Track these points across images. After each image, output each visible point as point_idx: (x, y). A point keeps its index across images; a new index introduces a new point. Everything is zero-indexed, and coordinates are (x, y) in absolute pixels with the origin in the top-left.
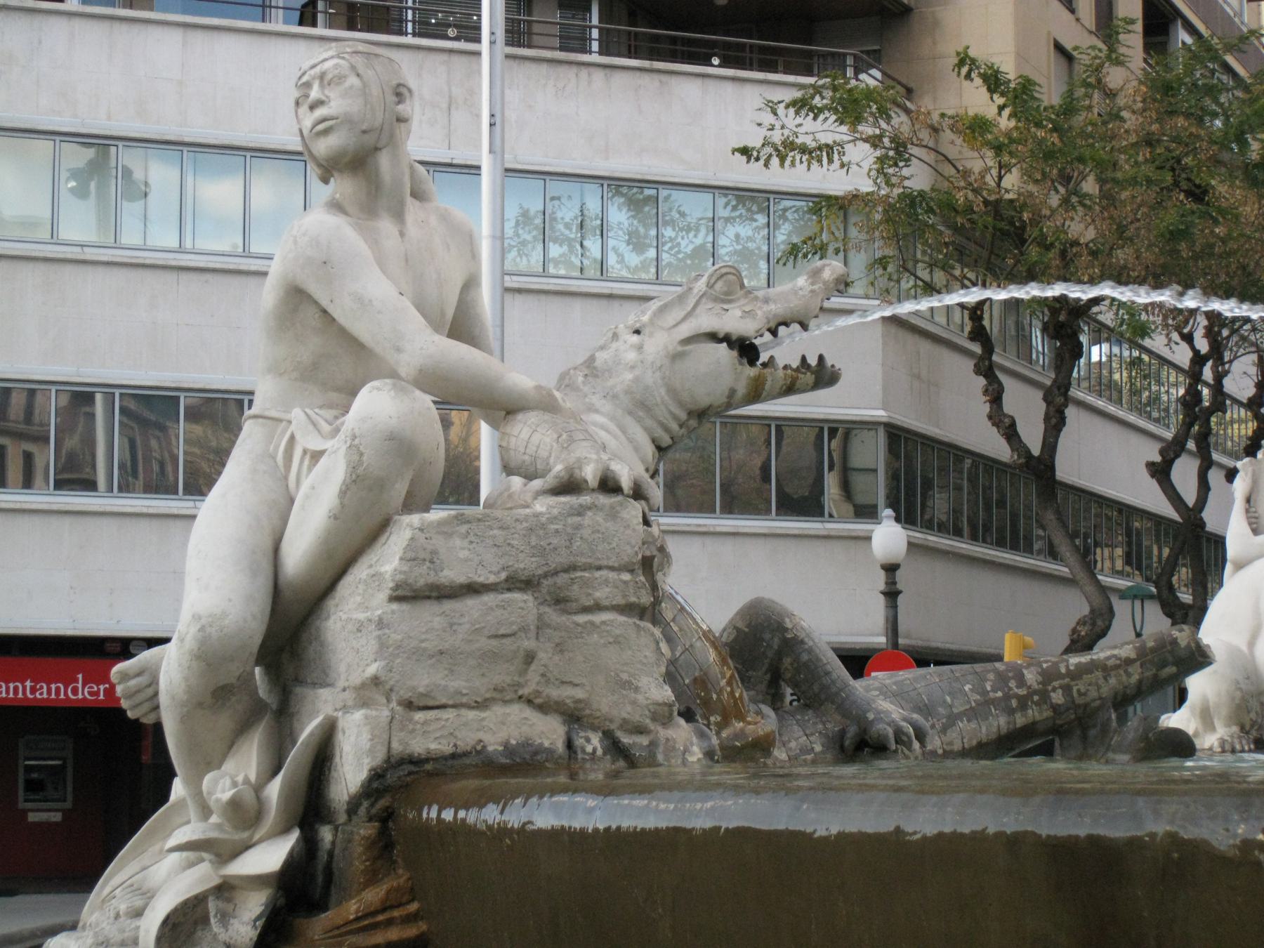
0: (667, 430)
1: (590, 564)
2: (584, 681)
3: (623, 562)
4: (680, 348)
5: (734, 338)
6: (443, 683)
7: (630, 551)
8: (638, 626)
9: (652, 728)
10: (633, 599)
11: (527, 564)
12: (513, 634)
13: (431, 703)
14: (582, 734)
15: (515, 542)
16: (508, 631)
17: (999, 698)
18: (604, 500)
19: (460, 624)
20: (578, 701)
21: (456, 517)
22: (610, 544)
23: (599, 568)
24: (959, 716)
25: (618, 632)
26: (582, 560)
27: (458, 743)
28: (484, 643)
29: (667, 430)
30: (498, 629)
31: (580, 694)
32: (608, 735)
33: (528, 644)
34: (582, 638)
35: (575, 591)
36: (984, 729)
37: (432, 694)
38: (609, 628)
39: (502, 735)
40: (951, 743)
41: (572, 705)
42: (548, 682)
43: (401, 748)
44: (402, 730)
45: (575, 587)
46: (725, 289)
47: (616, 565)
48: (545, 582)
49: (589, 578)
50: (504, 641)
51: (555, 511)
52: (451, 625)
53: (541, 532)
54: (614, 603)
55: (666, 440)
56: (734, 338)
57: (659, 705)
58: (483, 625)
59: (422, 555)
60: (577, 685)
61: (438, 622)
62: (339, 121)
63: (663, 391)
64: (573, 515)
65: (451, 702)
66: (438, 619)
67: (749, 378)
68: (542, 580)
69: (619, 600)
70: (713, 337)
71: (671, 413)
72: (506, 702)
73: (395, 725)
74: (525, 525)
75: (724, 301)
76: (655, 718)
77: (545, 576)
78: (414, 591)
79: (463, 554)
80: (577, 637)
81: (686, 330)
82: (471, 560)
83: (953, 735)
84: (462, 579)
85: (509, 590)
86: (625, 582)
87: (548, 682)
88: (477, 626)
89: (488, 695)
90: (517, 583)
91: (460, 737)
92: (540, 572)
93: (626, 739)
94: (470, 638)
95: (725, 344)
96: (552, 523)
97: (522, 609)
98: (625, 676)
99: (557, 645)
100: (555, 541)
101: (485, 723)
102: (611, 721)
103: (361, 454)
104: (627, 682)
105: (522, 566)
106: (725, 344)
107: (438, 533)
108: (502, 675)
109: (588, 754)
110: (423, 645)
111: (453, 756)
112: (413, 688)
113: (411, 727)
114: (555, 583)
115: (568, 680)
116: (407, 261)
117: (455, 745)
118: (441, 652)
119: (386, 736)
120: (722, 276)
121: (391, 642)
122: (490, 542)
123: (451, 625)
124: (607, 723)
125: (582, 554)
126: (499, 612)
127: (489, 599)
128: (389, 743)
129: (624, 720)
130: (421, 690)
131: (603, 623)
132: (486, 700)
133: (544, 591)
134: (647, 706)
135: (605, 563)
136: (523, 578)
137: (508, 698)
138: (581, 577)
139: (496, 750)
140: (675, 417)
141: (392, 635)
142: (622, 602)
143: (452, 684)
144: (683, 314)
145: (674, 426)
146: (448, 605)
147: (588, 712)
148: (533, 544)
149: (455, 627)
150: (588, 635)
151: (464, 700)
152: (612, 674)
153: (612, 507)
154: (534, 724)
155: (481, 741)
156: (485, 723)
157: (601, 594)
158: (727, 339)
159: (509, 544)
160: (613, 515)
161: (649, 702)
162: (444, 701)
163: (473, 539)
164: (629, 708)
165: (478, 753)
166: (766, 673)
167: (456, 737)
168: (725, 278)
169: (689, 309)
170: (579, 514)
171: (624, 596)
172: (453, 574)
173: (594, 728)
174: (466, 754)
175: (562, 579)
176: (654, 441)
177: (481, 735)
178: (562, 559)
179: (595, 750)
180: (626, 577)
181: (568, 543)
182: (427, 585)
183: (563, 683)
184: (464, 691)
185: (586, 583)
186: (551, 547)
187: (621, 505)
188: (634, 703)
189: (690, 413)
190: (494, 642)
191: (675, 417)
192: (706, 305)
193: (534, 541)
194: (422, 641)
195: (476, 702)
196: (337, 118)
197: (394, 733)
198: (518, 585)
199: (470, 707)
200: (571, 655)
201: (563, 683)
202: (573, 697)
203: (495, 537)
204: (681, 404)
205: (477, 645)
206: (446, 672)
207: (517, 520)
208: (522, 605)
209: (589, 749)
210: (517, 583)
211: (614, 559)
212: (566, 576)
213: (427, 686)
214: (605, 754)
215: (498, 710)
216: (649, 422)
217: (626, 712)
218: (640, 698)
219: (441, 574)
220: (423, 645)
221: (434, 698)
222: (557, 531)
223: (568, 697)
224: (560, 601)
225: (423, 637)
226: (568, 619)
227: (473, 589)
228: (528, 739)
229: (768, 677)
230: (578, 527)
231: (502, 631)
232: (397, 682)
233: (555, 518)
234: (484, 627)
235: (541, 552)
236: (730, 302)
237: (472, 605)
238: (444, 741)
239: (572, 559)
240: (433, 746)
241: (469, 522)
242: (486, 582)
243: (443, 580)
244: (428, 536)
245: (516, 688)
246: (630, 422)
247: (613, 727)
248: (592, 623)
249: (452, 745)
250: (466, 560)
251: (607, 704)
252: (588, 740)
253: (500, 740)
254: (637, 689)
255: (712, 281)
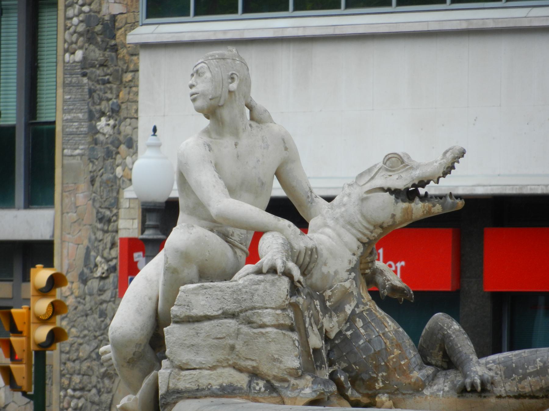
0: (364, 234)
1: (262, 306)
2: (256, 358)
3: (277, 306)
4: (365, 195)
5: (393, 189)
6: (193, 358)
7: (281, 301)
8: (284, 334)
9: (289, 379)
10: (282, 322)
11: (231, 307)
12: (224, 338)
13: (189, 367)
14: (255, 381)
15: (226, 297)
16: (222, 336)
17: (525, 367)
18: (270, 277)
19: (200, 333)
20: (253, 367)
21: (200, 286)
22: (272, 297)
23: (267, 308)
24: (530, 374)
25: (273, 336)
26: (258, 305)
27: (200, 385)
28: (211, 341)
29: (364, 234)
30: (217, 335)
31: (254, 364)
32: (268, 381)
33: (231, 342)
34: (257, 339)
35: (255, 319)
36: (543, 381)
37: (189, 363)
38: (269, 335)
39: (220, 381)
40: (524, 388)
41: (251, 369)
42: (240, 358)
43: (173, 386)
44: (174, 379)
45: (255, 317)
46: (391, 165)
47: (274, 307)
48: (241, 315)
49: (261, 313)
50: (220, 340)
51: (246, 283)
52: (197, 333)
53: (239, 293)
54: (272, 324)
55: (365, 240)
56: (393, 189)
57: (291, 369)
58: (210, 333)
59: (184, 303)
60: (253, 360)
61: (192, 332)
62: (199, 95)
63: (359, 216)
64: (254, 285)
65: (197, 367)
66: (191, 331)
67: (402, 208)
68: (240, 314)
69: (275, 322)
70: (382, 189)
71: (364, 226)
72: (224, 367)
73: (172, 376)
74: (231, 289)
75: (390, 171)
76: (290, 375)
77: (241, 311)
78: (181, 319)
79: (203, 303)
80: (255, 339)
81: (368, 187)
82: (206, 305)
83: (525, 383)
84: (201, 314)
85: (225, 318)
86: (278, 314)
87: (240, 358)
88: (208, 334)
89: (214, 364)
90: (227, 315)
91: (200, 382)
92: (238, 310)
93: (277, 384)
94: (205, 339)
95: (388, 192)
96: (244, 288)
97: (228, 326)
98: (276, 356)
99: (245, 342)
100: (245, 296)
101: (212, 376)
102: (269, 376)
103: (167, 258)
104: (277, 359)
105: (229, 308)
106: (388, 193)
107: (192, 293)
108: (220, 355)
109: (257, 390)
110: (185, 342)
111: (197, 390)
112: (180, 361)
113: (178, 377)
114: (246, 315)
115: (249, 358)
116: (238, 157)
117: (198, 386)
118: (193, 345)
119: (167, 381)
120: (389, 159)
121: (171, 341)
122: (214, 297)
123: (197, 333)
124: (267, 377)
125: (258, 302)
126: (218, 328)
127: (214, 322)
128: (168, 384)
129: (274, 375)
130: (184, 361)
131: (267, 332)
132: (214, 366)
133: (241, 319)
134: (285, 370)
135: (269, 306)
136: (230, 313)
137: (224, 365)
138: (257, 312)
139: (216, 388)
140: (367, 229)
141: (172, 338)
142: (276, 323)
143: (198, 359)
144: (370, 177)
145: (367, 232)
146: (196, 325)
147: (258, 372)
148: (235, 298)
149: (199, 334)
150: (260, 338)
151: (204, 366)
152: (270, 355)
153: (273, 281)
154: (234, 377)
155: (210, 384)
156: (212, 376)
157: (267, 320)
158: (389, 190)
159: (224, 298)
160: (273, 283)
161: (286, 368)
162: (195, 366)
163: (208, 296)
164: (276, 370)
165: (209, 389)
166: (439, 351)
167: (199, 382)
168: (390, 160)
169: (372, 175)
170: (258, 284)
171: (277, 320)
172: (197, 312)
173: (263, 379)
174: (203, 389)
175: (249, 313)
176: (359, 240)
177: (210, 381)
178: (248, 304)
179: (260, 388)
180: (279, 312)
181: (251, 297)
182: (186, 316)
183: (247, 359)
184: (203, 362)
185: (259, 315)
186: (243, 299)
187: (277, 279)
188: (279, 368)
189: (375, 227)
190: (215, 341)
191: (367, 229)
192: (383, 173)
193: (235, 296)
194: (185, 340)
195: (209, 367)
196: (198, 94)
197: (170, 380)
198: (230, 316)
199: (207, 369)
200: (251, 346)
201: (247, 359)
202: (251, 365)
203: (217, 295)
204: (369, 222)
205: (208, 342)
206: (195, 354)
207: (228, 287)
208: (228, 325)
209: (258, 388)
210: (227, 315)
211: (273, 304)
212: (250, 312)
213: (187, 360)
214: (266, 390)
215: (219, 370)
216: (354, 231)
217: (275, 372)
218: (282, 366)
219: (192, 311)
220: (185, 342)
221: (190, 365)
222: (246, 292)
223: (248, 365)
224: (250, 323)
225: (185, 338)
226: (251, 331)
227: (208, 318)
228: (231, 383)
229: (441, 353)
230: (257, 290)
231: (219, 336)
232: (174, 358)
233: (246, 286)
234: (211, 334)
235: (237, 301)
236: (394, 171)
237: (206, 325)
238: (193, 384)
239: (253, 304)
240: (188, 386)
241: (206, 289)
242: (212, 315)
243: (192, 314)
244: (187, 295)
245: (227, 361)
246: (343, 231)
247: (269, 378)
248: (262, 333)
249: (197, 385)
250: (204, 305)
251: (265, 368)
252: (257, 384)
253: (218, 384)
254: (281, 362)
255: (385, 161)
